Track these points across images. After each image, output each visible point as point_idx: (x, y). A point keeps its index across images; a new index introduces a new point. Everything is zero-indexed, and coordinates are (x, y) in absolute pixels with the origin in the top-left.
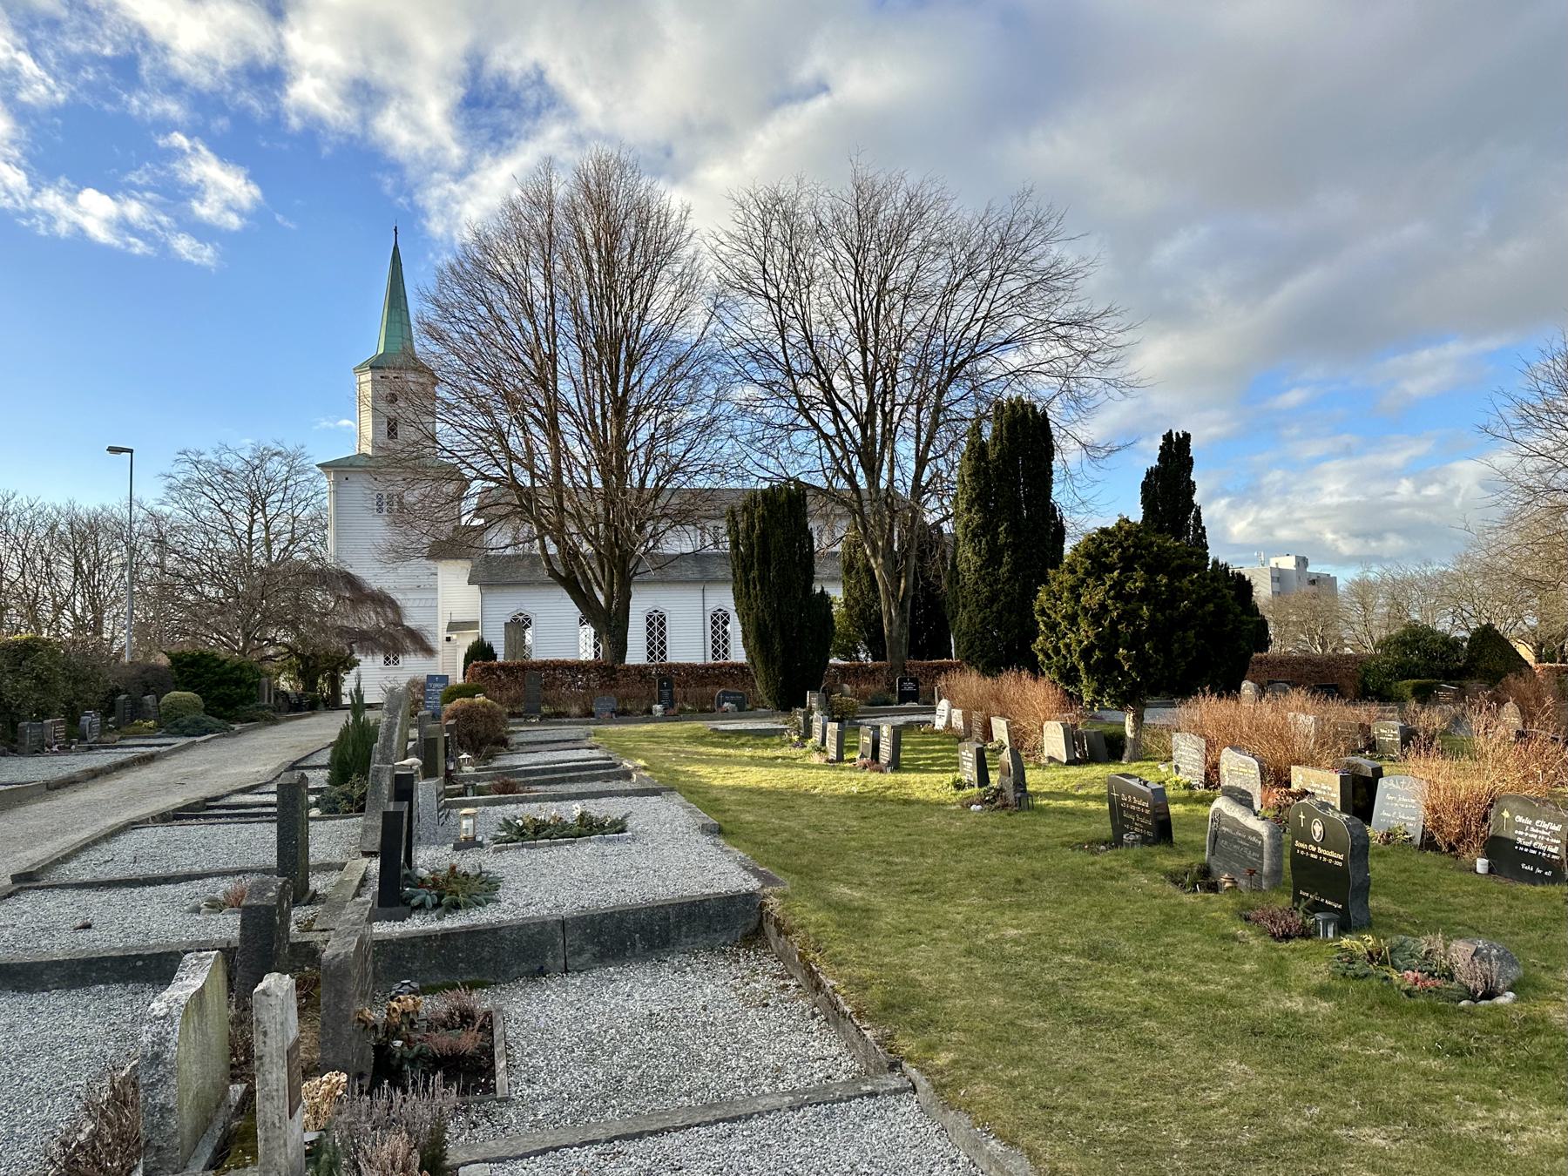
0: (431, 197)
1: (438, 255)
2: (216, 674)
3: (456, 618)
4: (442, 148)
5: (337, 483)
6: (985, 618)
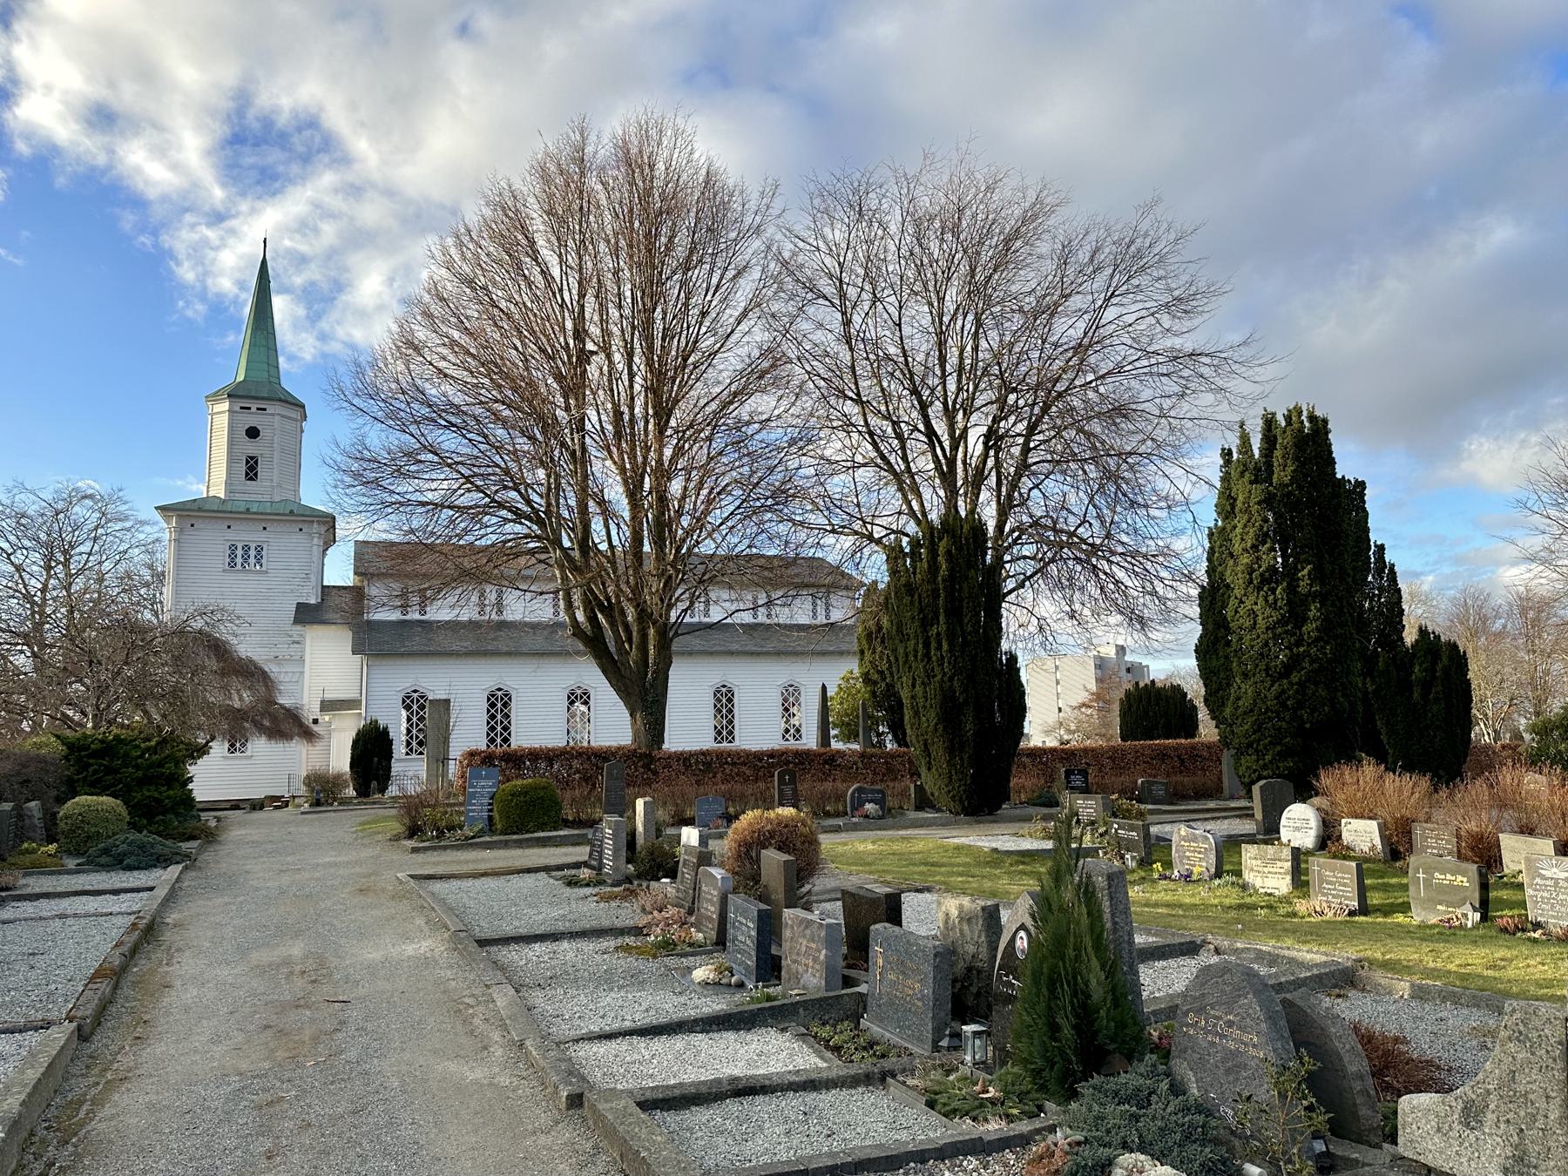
0: (182, 238)
1: (188, 303)
2: (137, 767)
3: (329, 696)
4: (196, 185)
5: (180, 530)
6: (1283, 692)
